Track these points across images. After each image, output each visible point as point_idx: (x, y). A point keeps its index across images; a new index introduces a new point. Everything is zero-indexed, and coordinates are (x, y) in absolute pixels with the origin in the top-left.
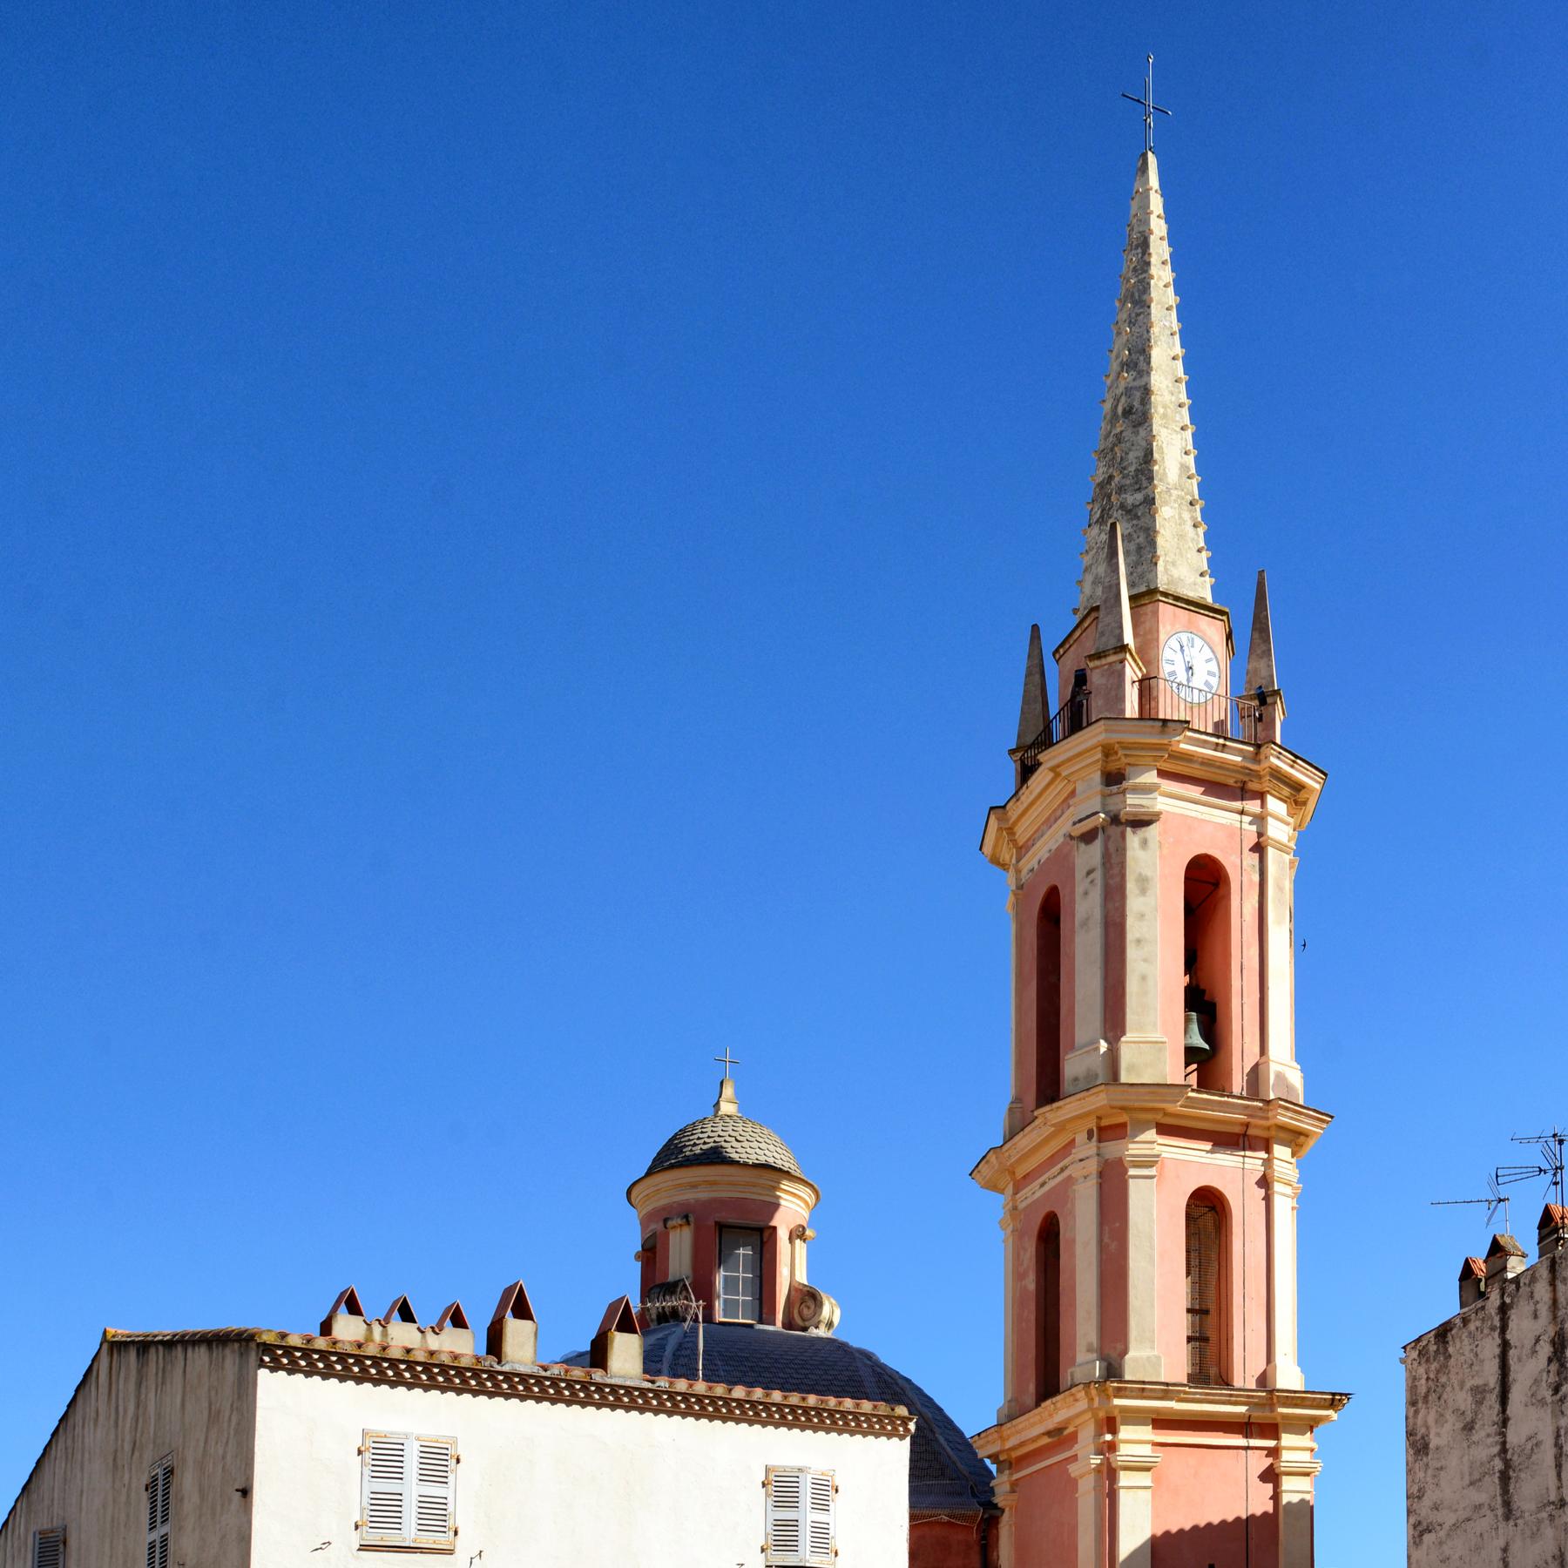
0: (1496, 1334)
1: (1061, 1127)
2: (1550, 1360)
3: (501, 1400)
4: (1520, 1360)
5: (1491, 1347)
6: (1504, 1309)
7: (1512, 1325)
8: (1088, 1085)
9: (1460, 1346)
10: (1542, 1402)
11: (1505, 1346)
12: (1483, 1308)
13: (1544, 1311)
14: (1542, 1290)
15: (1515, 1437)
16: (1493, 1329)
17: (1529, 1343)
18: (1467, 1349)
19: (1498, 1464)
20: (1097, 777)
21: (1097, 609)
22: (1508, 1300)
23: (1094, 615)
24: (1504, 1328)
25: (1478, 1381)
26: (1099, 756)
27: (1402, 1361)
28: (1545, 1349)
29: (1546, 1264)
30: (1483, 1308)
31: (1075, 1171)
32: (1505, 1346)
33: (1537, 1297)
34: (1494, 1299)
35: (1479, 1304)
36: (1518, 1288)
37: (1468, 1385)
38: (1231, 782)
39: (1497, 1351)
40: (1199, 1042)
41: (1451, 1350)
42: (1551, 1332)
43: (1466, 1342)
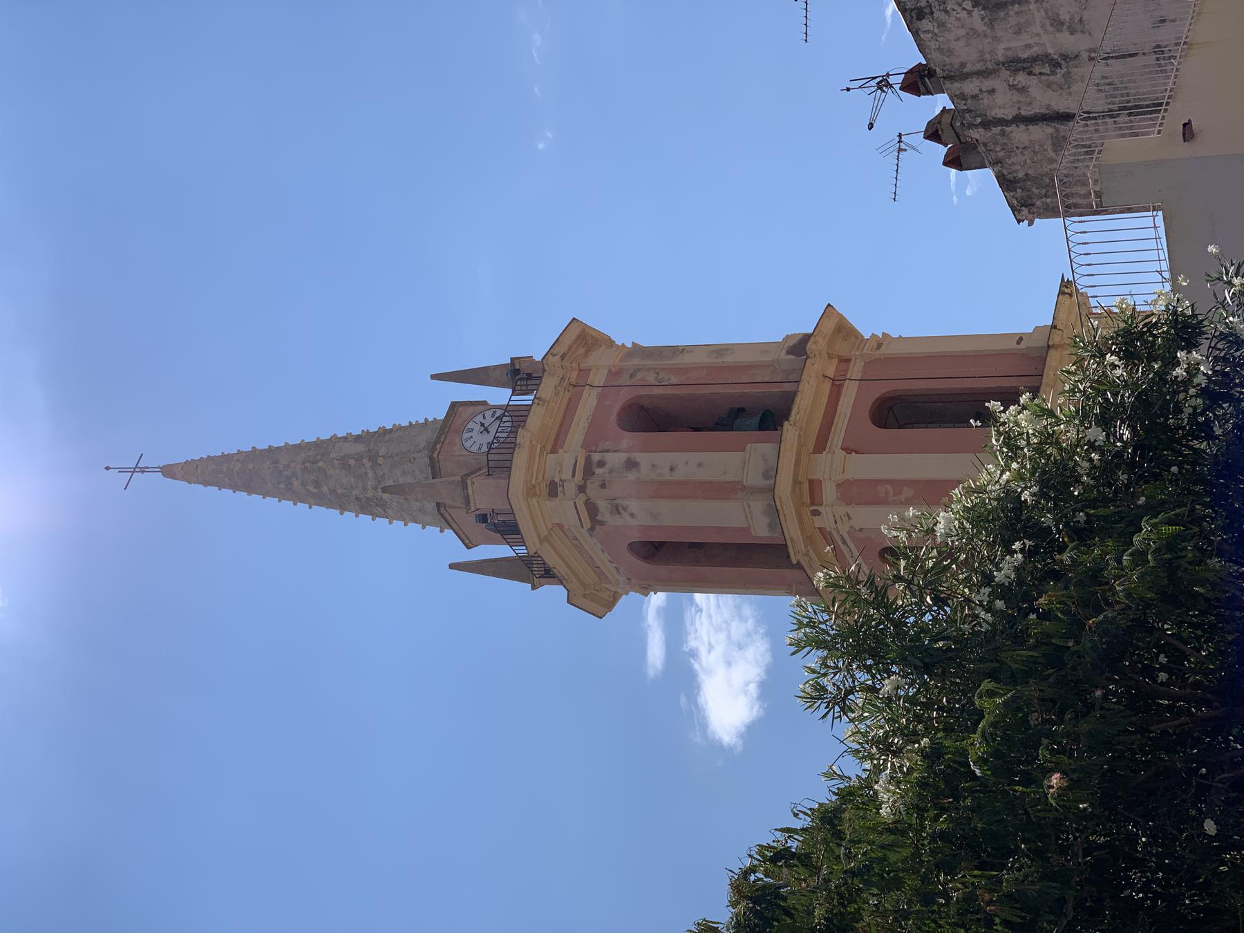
0: (1007, 129)
1: (809, 540)
2: (1030, 73)
3: (645, 343)
4: (1030, 104)
5: (1019, 134)
6: (986, 124)
7: (999, 113)
8: (774, 512)
9: (1019, 166)
10: (1067, 76)
11: (1019, 120)
12: (985, 145)
13: (988, 84)
14: (970, 87)
15: (1097, 102)
16: (1003, 133)
17: (1016, 97)
18: (1020, 158)
19: (1123, 118)
20: (551, 504)
21: (438, 504)
22: (979, 120)
23: (442, 510)
24: (1002, 122)
25: (1048, 145)
26: (534, 500)
27: (1031, 224)
28: (1022, 78)
29: (948, 85)
30: (985, 145)
31: (844, 529)
32: (1019, 120)
33: (976, 91)
34: (976, 134)
35: (981, 149)
36: (969, 111)
37: (1052, 154)
38: (567, 395)
39: (1022, 127)
40: (755, 420)
41: (1021, 175)
42: (1005, 73)
43: (1014, 159)
